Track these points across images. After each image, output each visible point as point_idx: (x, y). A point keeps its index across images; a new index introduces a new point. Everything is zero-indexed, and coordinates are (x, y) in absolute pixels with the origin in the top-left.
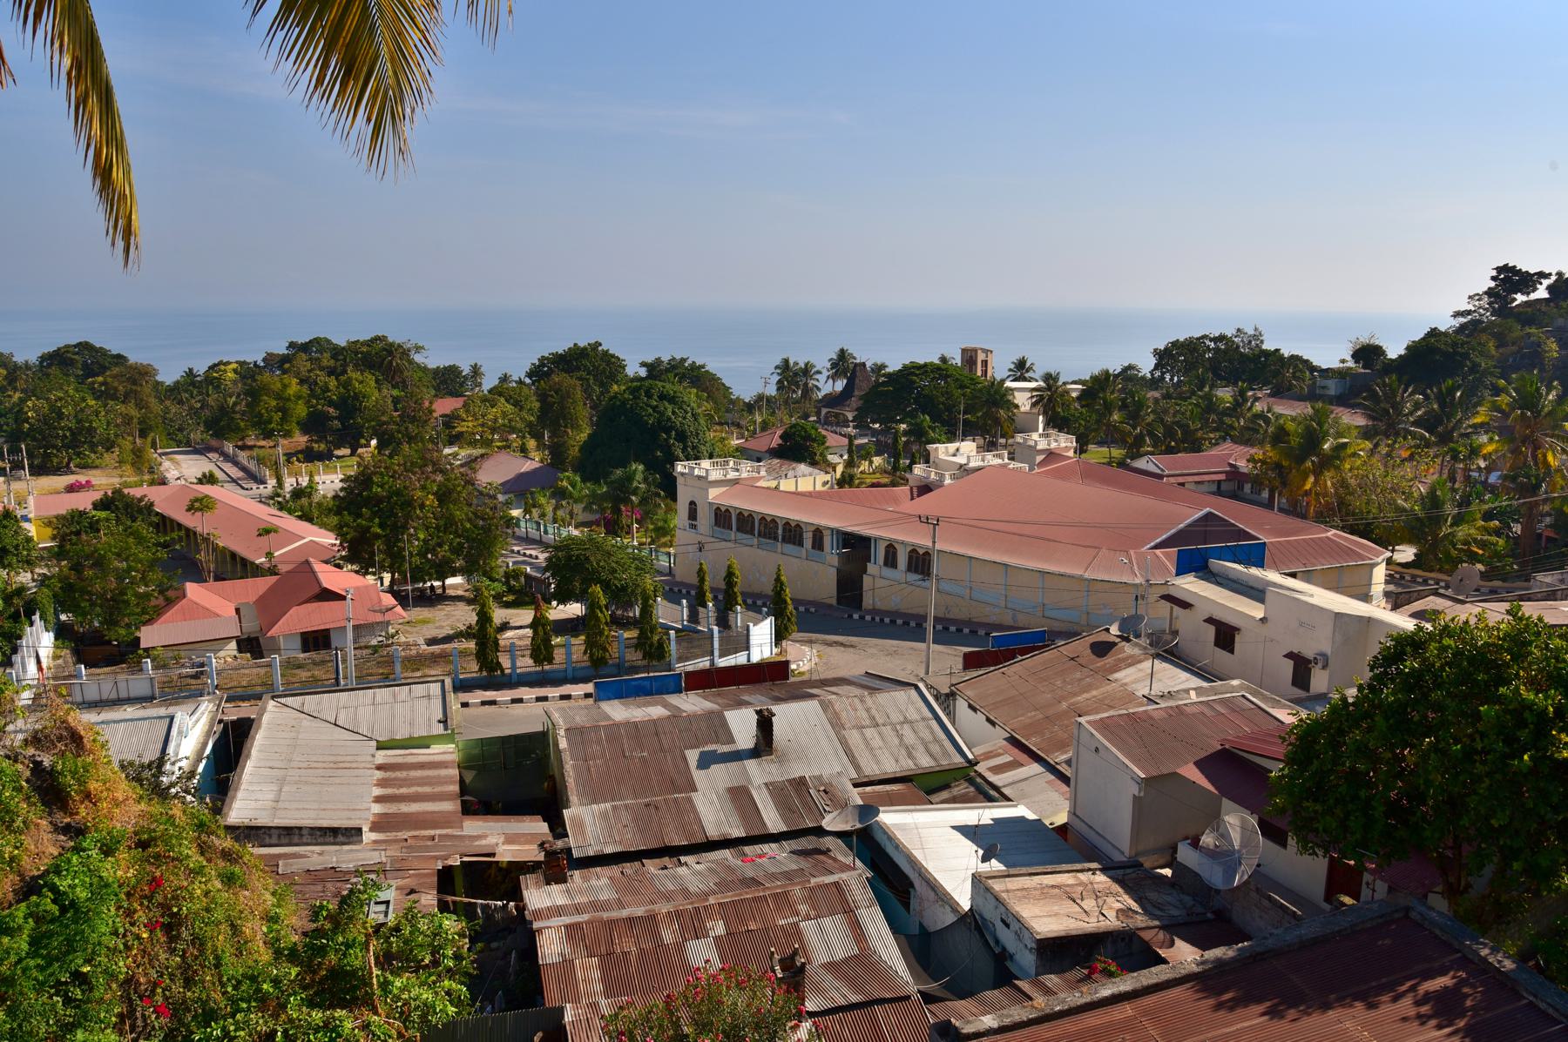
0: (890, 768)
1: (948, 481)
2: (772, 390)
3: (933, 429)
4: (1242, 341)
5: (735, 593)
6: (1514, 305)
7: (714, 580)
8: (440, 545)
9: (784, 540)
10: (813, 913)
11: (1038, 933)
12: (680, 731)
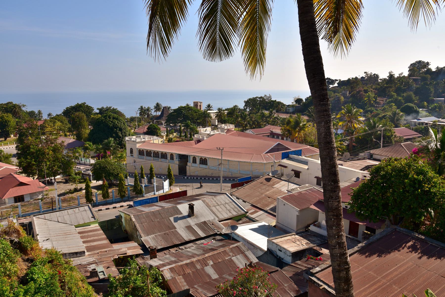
0: (226, 216)
1: (205, 139)
3: (192, 125)
4: (266, 98)
5: (153, 174)
6: (330, 88)
7: (146, 171)
8: (54, 166)
9: (161, 158)
10: (234, 255)
11: (291, 251)
12: (166, 212)
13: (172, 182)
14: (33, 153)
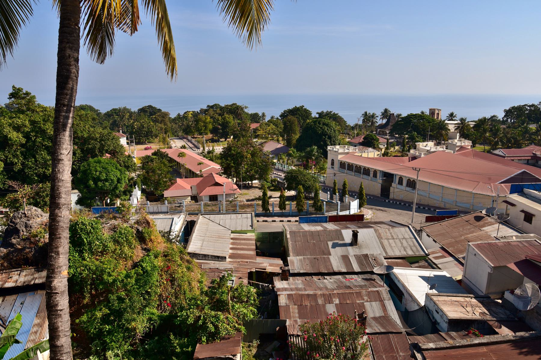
0: (398, 254)
1: (423, 156)
2: (360, 123)
3: (418, 137)
5: (346, 191)
7: (339, 186)
10: (369, 300)
11: (449, 317)
12: (326, 235)
13: (363, 204)
14: (233, 155)
